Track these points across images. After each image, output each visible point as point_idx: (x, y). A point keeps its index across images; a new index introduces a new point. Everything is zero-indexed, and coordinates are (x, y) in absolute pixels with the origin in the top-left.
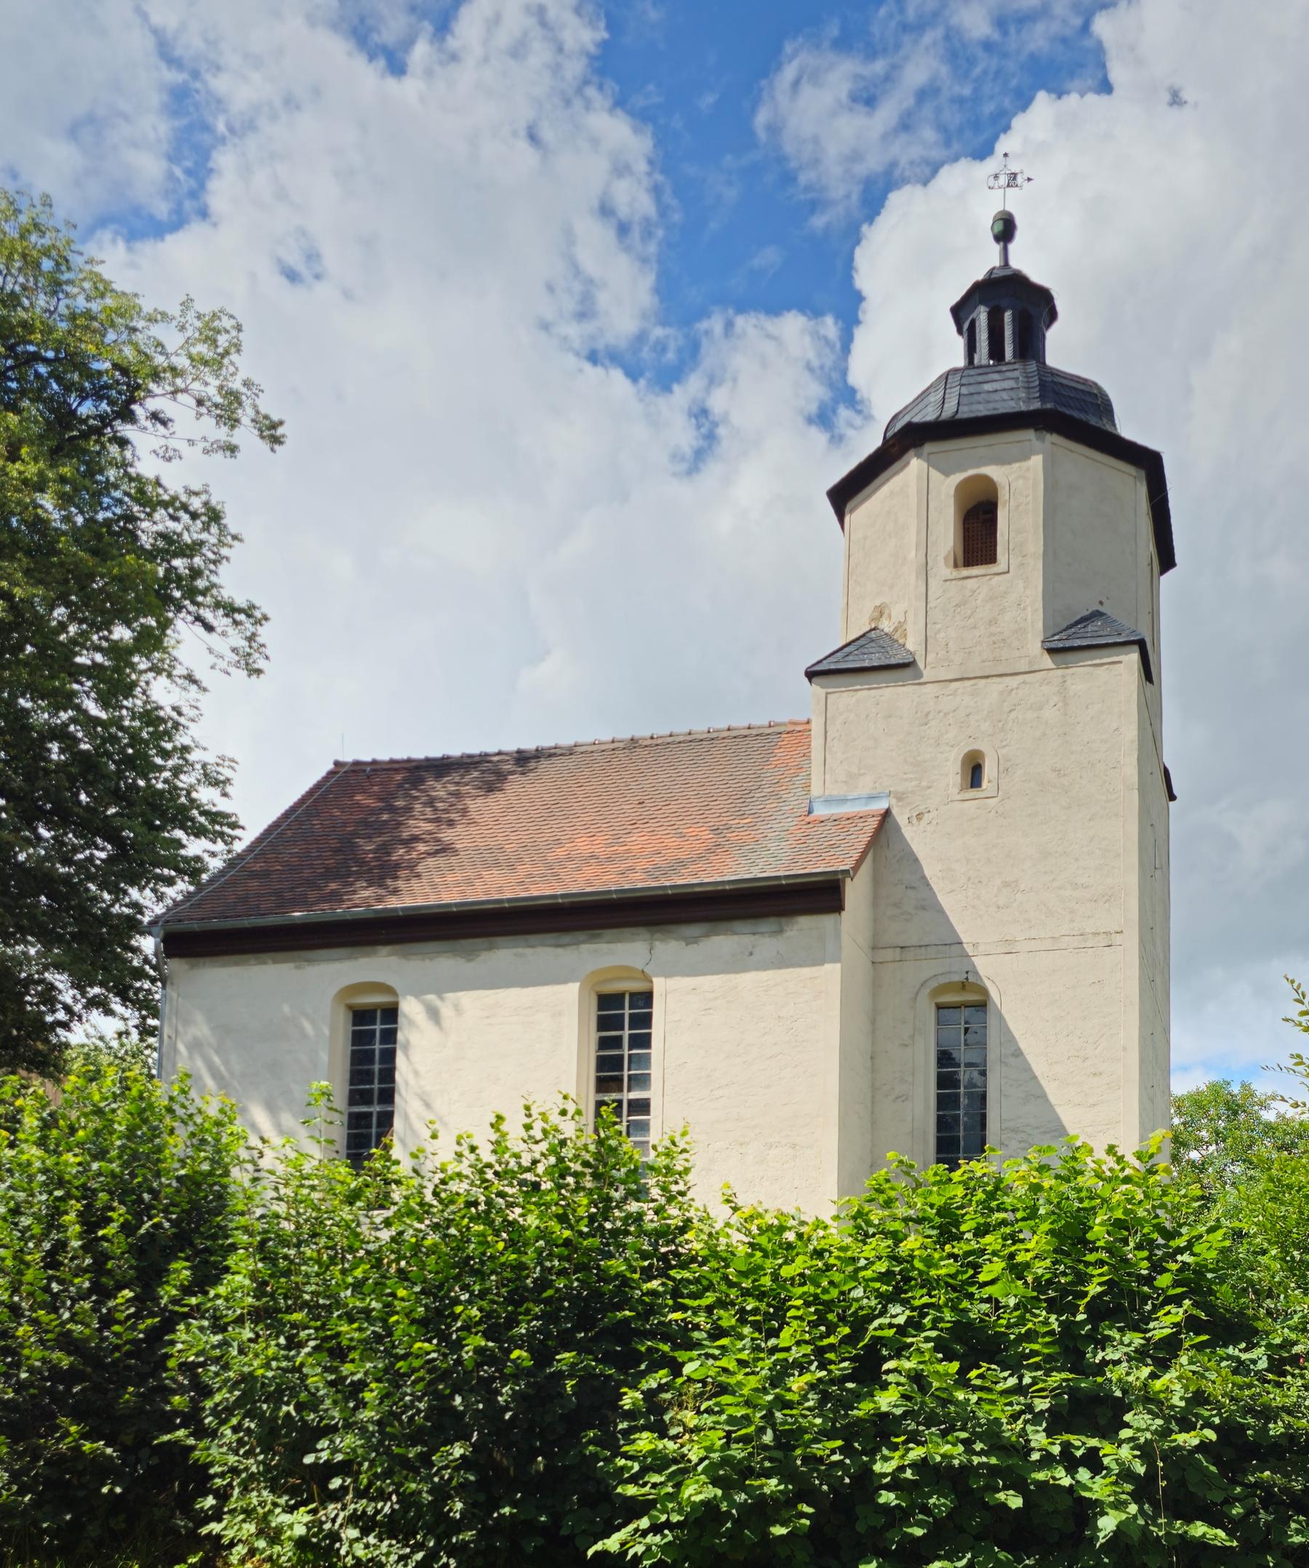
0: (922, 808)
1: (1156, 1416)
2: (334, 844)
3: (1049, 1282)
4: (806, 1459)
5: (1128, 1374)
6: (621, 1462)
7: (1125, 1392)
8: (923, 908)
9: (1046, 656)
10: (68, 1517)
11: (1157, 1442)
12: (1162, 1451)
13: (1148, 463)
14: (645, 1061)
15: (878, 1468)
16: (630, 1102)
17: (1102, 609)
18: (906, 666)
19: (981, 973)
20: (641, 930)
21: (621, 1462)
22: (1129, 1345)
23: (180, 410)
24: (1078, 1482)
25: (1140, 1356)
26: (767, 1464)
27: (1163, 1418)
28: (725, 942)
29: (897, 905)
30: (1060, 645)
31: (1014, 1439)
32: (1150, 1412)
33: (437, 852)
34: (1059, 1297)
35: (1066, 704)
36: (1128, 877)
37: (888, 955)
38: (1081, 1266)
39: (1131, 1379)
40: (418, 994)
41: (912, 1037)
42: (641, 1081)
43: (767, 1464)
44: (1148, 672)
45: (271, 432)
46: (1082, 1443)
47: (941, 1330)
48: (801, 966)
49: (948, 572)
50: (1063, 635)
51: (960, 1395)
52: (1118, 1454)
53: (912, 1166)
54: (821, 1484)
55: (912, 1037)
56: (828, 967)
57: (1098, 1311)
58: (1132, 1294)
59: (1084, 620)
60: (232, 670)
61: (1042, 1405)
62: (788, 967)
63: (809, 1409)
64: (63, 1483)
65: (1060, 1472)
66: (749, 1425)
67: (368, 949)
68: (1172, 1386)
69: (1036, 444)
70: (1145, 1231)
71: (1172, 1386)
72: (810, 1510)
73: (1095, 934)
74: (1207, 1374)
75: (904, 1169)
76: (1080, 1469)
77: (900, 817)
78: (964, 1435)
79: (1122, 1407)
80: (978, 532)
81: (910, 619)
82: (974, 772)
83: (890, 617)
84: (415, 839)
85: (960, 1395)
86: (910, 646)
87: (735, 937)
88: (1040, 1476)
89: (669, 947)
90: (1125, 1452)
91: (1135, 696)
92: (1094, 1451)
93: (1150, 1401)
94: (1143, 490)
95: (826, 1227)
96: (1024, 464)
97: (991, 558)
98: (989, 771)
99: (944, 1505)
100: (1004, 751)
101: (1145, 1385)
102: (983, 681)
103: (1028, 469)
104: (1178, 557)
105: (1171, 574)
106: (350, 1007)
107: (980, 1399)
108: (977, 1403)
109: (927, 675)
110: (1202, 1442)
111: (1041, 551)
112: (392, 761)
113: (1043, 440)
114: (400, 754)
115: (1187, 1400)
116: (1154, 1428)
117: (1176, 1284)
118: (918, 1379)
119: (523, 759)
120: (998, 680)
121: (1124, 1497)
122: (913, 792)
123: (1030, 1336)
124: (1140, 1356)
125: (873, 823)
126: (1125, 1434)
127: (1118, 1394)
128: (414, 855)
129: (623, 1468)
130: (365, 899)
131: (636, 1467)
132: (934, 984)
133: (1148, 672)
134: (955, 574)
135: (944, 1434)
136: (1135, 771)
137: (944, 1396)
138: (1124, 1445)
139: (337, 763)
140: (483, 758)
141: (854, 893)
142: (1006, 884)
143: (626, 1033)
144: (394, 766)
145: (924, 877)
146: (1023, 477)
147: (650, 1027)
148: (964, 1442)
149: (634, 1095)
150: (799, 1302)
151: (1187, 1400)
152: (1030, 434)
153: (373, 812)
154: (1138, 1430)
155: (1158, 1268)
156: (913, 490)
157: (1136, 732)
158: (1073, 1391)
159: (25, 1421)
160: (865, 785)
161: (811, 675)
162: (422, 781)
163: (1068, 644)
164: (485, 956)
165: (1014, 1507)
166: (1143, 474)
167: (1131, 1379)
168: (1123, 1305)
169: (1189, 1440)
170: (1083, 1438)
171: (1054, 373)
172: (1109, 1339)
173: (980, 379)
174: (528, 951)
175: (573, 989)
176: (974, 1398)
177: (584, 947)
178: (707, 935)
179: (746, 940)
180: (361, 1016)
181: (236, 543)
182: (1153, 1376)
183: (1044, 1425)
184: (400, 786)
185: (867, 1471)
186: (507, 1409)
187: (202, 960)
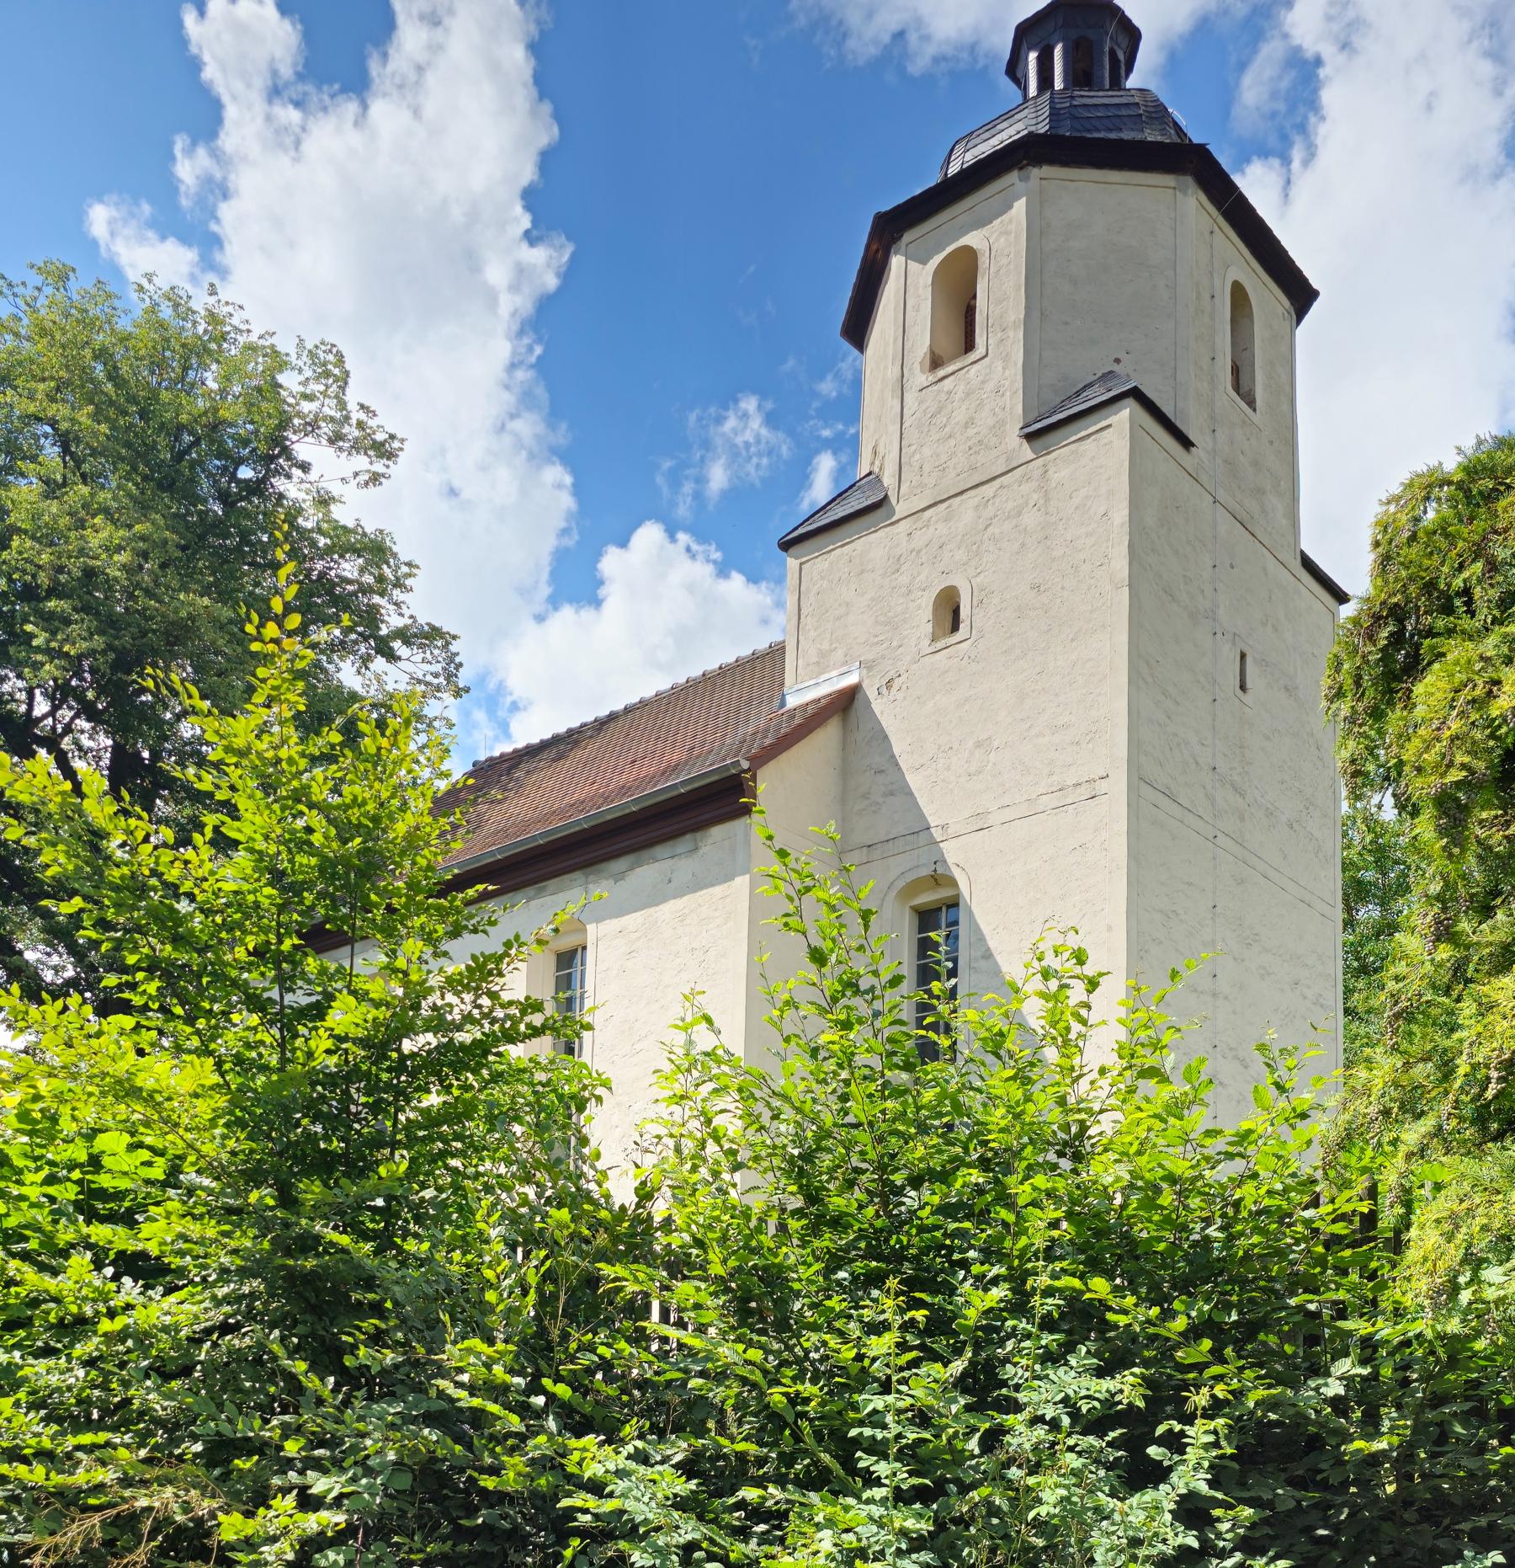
0: (892, 674)
8: (892, 794)
19: (950, 861)
20: (577, 875)
28: (647, 871)
29: (865, 796)
35: (1047, 500)
37: (857, 857)
56: (738, 880)
59: (1078, 393)
69: (1020, 186)
82: (949, 613)
109: (900, 509)
132: (901, 884)
136: (1125, 562)
152: (1013, 177)
166: (1189, 180)
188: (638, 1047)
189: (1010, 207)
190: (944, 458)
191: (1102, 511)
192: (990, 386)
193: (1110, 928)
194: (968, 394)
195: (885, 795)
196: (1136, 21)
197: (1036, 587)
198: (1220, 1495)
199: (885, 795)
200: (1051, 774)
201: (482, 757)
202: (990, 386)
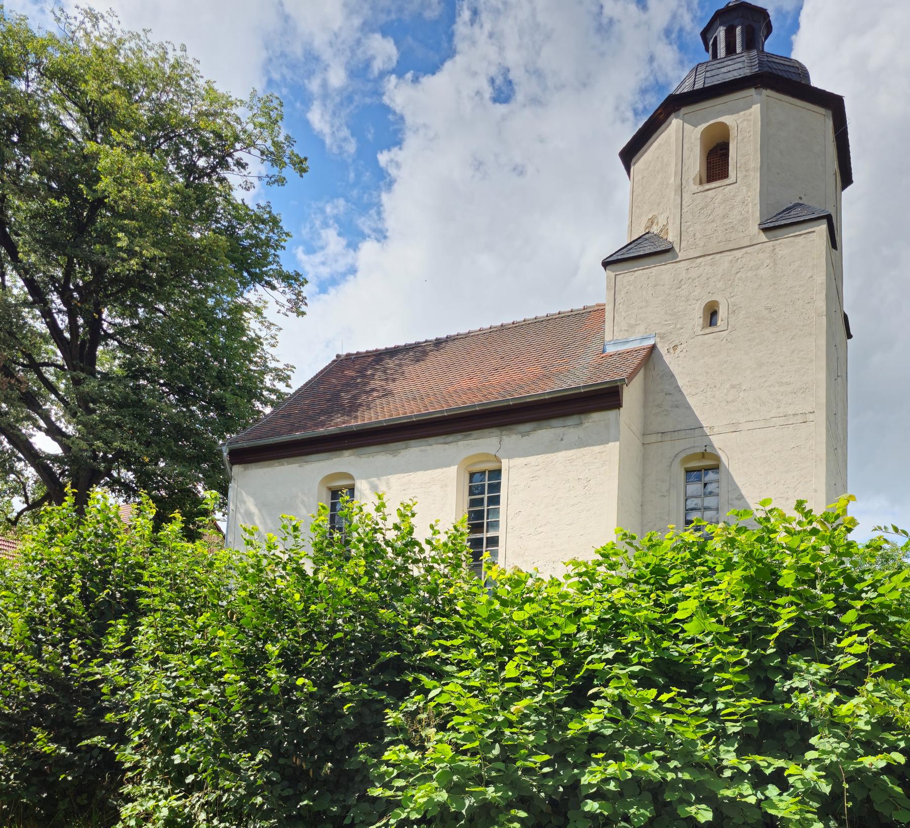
0: (676, 342)
1: (841, 739)
2: (328, 397)
3: (744, 622)
4: (527, 771)
5: (813, 700)
6: (384, 768)
7: (811, 717)
9: (762, 234)
10: (45, 795)
11: (842, 763)
12: (846, 772)
13: (833, 104)
14: (497, 511)
15: (585, 780)
16: (487, 538)
17: (801, 202)
18: (666, 252)
19: (716, 446)
21: (384, 768)
22: (815, 674)
23: (251, 158)
24: (767, 798)
25: (827, 684)
26: (494, 774)
27: (849, 741)
28: (545, 433)
29: (659, 406)
30: (771, 225)
31: (706, 757)
32: (835, 736)
33: (383, 396)
34: (749, 633)
35: (775, 264)
36: (819, 375)
37: (653, 438)
38: (771, 607)
39: (817, 704)
40: (366, 478)
41: (668, 491)
42: (495, 525)
43: (494, 774)
44: (834, 241)
45: (300, 166)
46: (769, 764)
47: (644, 664)
48: (594, 445)
49: (696, 188)
50: (774, 219)
51: (656, 718)
52: (804, 774)
53: (633, 538)
54: (539, 792)
55: (668, 491)
56: (611, 444)
57: (786, 646)
58: (818, 633)
59: (789, 209)
60: (289, 313)
61: (733, 728)
62: (585, 446)
63: (527, 728)
64: (38, 771)
65: (746, 788)
66: (475, 741)
67: (338, 453)
68: (858, 710)
70: (832, 575)
71: (858, 710)
72: (522, 814)
73: (794, 415)
74: (893, 701)
75: (628, 540)
76: (770, 786)
77: (662, 349)
78: (660, 753)
79: (808, 731)
80: (716, 161)
81: (670, 222)
82: (711, 315)
83: (658, 223)
84: (373, 390)
85: (656, 718)
86: (670, 239)
87: (552, 430)
88: (729, 793)
89: (511, 439)
90: (810, 773)
91: (824, 253)
92: (781, 770)
93: (834, 723)
94: (830, 123)
95: (560, 584)
96: (747, 112)
97: (724, 175)
98: (722, 313)
99: (643, 815)
100: (732, 300)
101: (831, 711)
102: (719, 255)
103: (750, 114)
104: (855, 177)
105: (849, 188)
106: (329, 489)
107: (674, 721)
108: (672, 725)
109: (681, 255)
110: (889, 764)
111: (759, 166)
112: (367, 352)
113: (761, 94)
114: (372, 348)
115: (872, 725)
116: (839, 751)
117: (860, 620)
118: (621, 703)
119: (438, 343)
120: (728, 253)
121: (809, 816)
122: (671, 333)
123: (722, 667)
124: (827, 684)
125: (644, 353)
126: (810, 755)
127: (805, 719)
128: (370, 398)
129: (386, 773)
130: (339, 423)
131: (396, 773)
132: (683, 455)
133: (834, 241)
134: (701, 188)
135: (642, 752)
137: (642, 718)
138: (810, 766)
139: (338, 356)
140: (417, 345)
141: (631, 395)
142: (733, 387)
143: (486, 496)
144: (368, 354)
145: (678, 386)
146: (746, 121)
147: (499, 491)
148: (659, 760)
149: (490, 535)
150: (523, 641)
151: (872, 725)
152: (752, 91)
153: (353, 378)
154: (824, 752)
155: (843, 608)
156: (673, 139)
157: (824, 277)
158: (764, 717)
159: (14, 730)
160: (640, 331)
161: (606, 264)
162: (382, 360)
163: (777, 224)
164: (403, 452)
165: (702, 820)
166: (830, 113)
167: (817, 704)
168: (809, 639)
169: (875, 762)
170: (770, 760)
171: (769, 55)
172: (795, 669)
173: (719, 66)
174: (428, 448)
175: (453, 471)
176: (669, 720)
177: (461, 443)
178: (535, 430)
179: (559, 431)
180: (335, 494)
181: (288, 238)
182: (838, 702)
183: (736, 746)
184: (370, 364)
185: (574, 786)
186: (305, 725)
187: (250, 465)
188: (540, 530)
190: (709, 232)
191: (809, 274)
192: (739, 199)
193: (816, 491)
197: (769, 309)
198: (126, 649)
200: (778, 407)
202: (739, 199)
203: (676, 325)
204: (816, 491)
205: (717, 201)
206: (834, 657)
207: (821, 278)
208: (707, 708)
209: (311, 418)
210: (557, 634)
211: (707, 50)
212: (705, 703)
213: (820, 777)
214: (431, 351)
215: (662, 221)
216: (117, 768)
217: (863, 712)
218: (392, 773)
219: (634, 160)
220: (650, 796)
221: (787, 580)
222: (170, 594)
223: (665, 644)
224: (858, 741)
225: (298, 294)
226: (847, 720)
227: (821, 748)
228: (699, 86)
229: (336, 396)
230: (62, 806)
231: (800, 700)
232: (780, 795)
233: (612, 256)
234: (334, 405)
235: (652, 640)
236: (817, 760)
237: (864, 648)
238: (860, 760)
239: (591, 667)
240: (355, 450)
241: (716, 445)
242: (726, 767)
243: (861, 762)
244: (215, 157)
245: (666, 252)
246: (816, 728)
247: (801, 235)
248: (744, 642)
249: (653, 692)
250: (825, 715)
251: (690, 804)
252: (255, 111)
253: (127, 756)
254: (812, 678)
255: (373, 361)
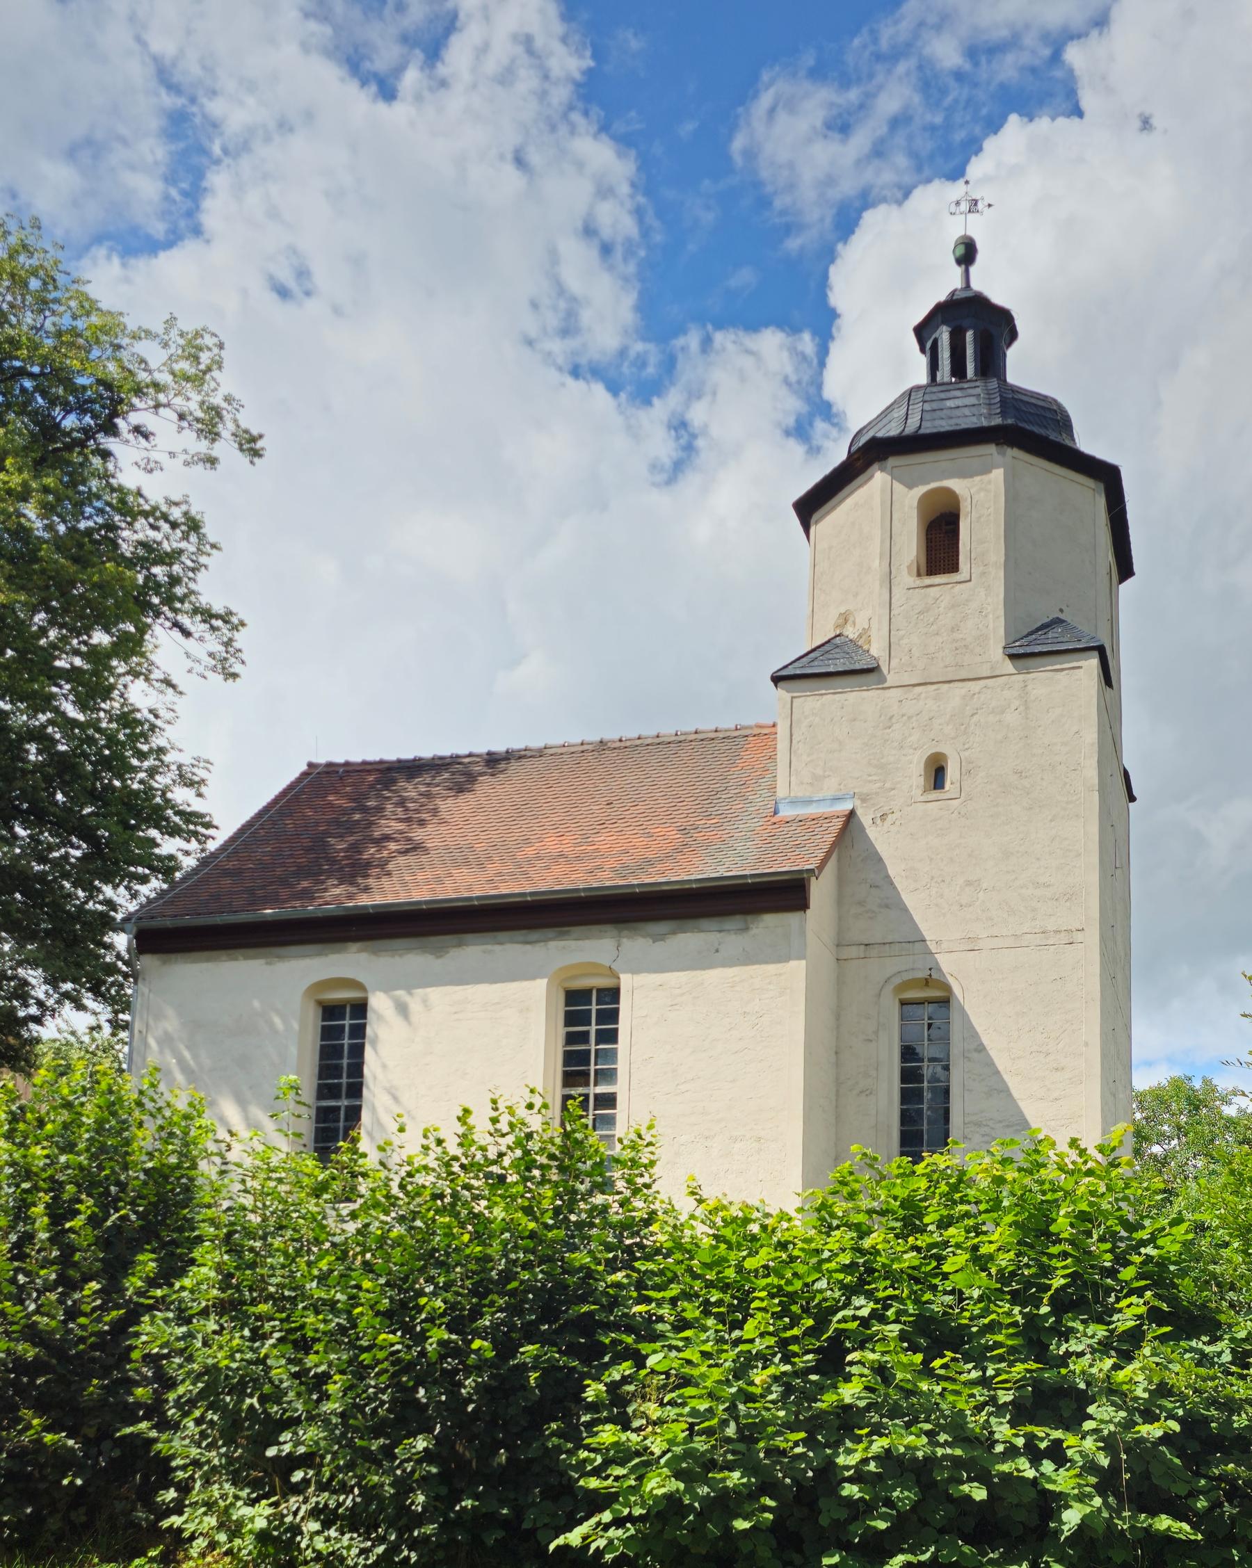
1: (1119, 1408)
2: (307, 843)
3: (1013, 1274)
5: (1091, 1366)
6: (584, 1454)
7: (1088, 1384)
8: (887, 906)
9: (1008, 661)
10: (29, 1511)
12: (1124, 1442)
13: (1107, 477)
14: (612, 1056)
15: (841, 1460)
16: (597, 1096)
17: (1062, 616)
18: (868, 672)
21: (584, 1454)
22: (1092, 1337)
23: (162, 424)
24: (1042, 1474)
25: (1104, 1347)
26: (730, 1457)
28: (691, 939)
29: (861, 903)
32: (1113, 1404)
35: (1027, 708)
37: (853, 952)
39: (1094, 1370)
40: (387, 989)
41: (876, 1033)
42: (608, 1076)
43: (730, 1457)
44: (1107, 677)
45: (250, 445)
46: (1046, 1434)
47: (905, 1323)
48: (767, 963)
49: (912, 580)
50: (1024, 642)
51: (924, 1386)
52: (1081, 1446)
53: (875, 1159)
55: (876, 1033)
56: (793, 963)
57: (1062, 1304)
60: (209, 674)
61: (1005, 1397)
62: (753, 963)
65: (1023, 1463)
67: (338, 946)
68: (1135, 1377)
71: (1135, 1377)
74: (1170, 1366)
75: (868, 1161)
77: (865, 817)
78: (927, 1427)
79: (1084, 1399)
80: (941, 542)
81: (874, 626)
82: (937, 774)
84: (387, 838)
85: (924, 1386)
86: (874, 651)
87: (702, 935)
90: (1089, 1444)
92: (1058, 1443)
93: (1113, 1392)
94: (1102, 502)
97: (953, 567)
98: (952, 773)
99: (907, 1498)
100: (967, 753)
102: (946, 686)
103: (989, 482)
105: (1130, 582)
109: (891, 680)
112: (364, 763)
113: (1004, 454)
114: (373, 755)
115: (1150, 1392)
116: (1117, 1420)
118: (881, 1371)
119: (493, 761)
122: (877, 794)
123: (992, 1328)
124: (1104, 1347)
125: (838, 824)
126: (1088, 1425)
127: (1082, 1386)
128: (385, 853)
129: (585, 1460)
130: (335, 896)
133: (1107, 677)
134: (919, 582)
139: (310, 765)
140: (455, 760)
141: (820, 891)
142: (969, 883)
143: (593, 1028)
144: (366, 768)
145: (888, 876)
146: (985, 491)
147: (616, 1022)
149: (601, 1089)
151: (1150, 1392)
152: (990, 449)
153: (345, 812)
154: (1102, 1421)
155: (1122, 1260)
157: (1096, 735)
158: (1037, 1383)
160: (830, 787)
161: (777, 679)
163: (1029, 650)
165: (978, 1499)
166: (1101, 486)
168: (1086, 1298)
170: (1047, 1430)
171: (1015, 390)
172: (1072, 1330)
173: (943, 395)
174: (497, 948)
175: (540, 986)
177: (552, 944)
178: (674, 933)
180: (331, 1011)
181: (214, 552)
182: (1116, 1367)
183: (1008, 1417)
184: (372, 786)
186: (470, 1401)
187: (173, 956)
189: (990, 472)
194: (953, 606)
195: (880, 906)
196: (1019, 328)
199: (880, 906)
200: (1034, 919)
201: (321, 759)
203: (885, 782)
204: (1086, 1044)
205: (943, 605)
206: (1111, 1316)
207: (1091, 735)
208: (975, 1374)
209: (284, 882)
210: (798, 1285)
211: (923, 350)
212: (974, 1368)
213: (1099, 1448)
214: (481, 774)
215: (861, 622)
216: (162, 1470)
217: (1140, 1378)
218: (595, 1460)
219: (815, 517)
220: (913, 1477)
221: (1062, 1224)
222: (661, 1312)
223: (928, 1296)
224: (1137, 1409)
225: (228, 643)
226: (1125, 1387)
227: (1099, 1417)
228: (912, 425)
229: (319, 845)
230: (54, 1523)
231: (1077, 1366)
232: (1056, 1470)
233: (786, 667)
234: (318, 862)
235: (913, 1292)
236: (1095, 1431)
237: (1142, 1310)
238: (1137, 1428)
239: (843, 1326)
240: (369, 943)
241: (945, 968)
242: (997, 1441)
243: (1139, 1432)
244: (95, 416)
245: (868, 672)
246: (1094, 1396)
247: (1063, 670)
248: (1016, 1298)
249: (918, 1358)
250: (1103, 1382)
251: (963, 1483)
252: (172, 350)
253: (181, 1446)
254: (1089, 1341)
255: (378, 781)
